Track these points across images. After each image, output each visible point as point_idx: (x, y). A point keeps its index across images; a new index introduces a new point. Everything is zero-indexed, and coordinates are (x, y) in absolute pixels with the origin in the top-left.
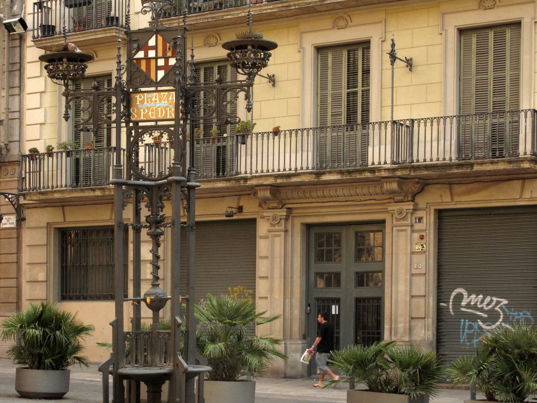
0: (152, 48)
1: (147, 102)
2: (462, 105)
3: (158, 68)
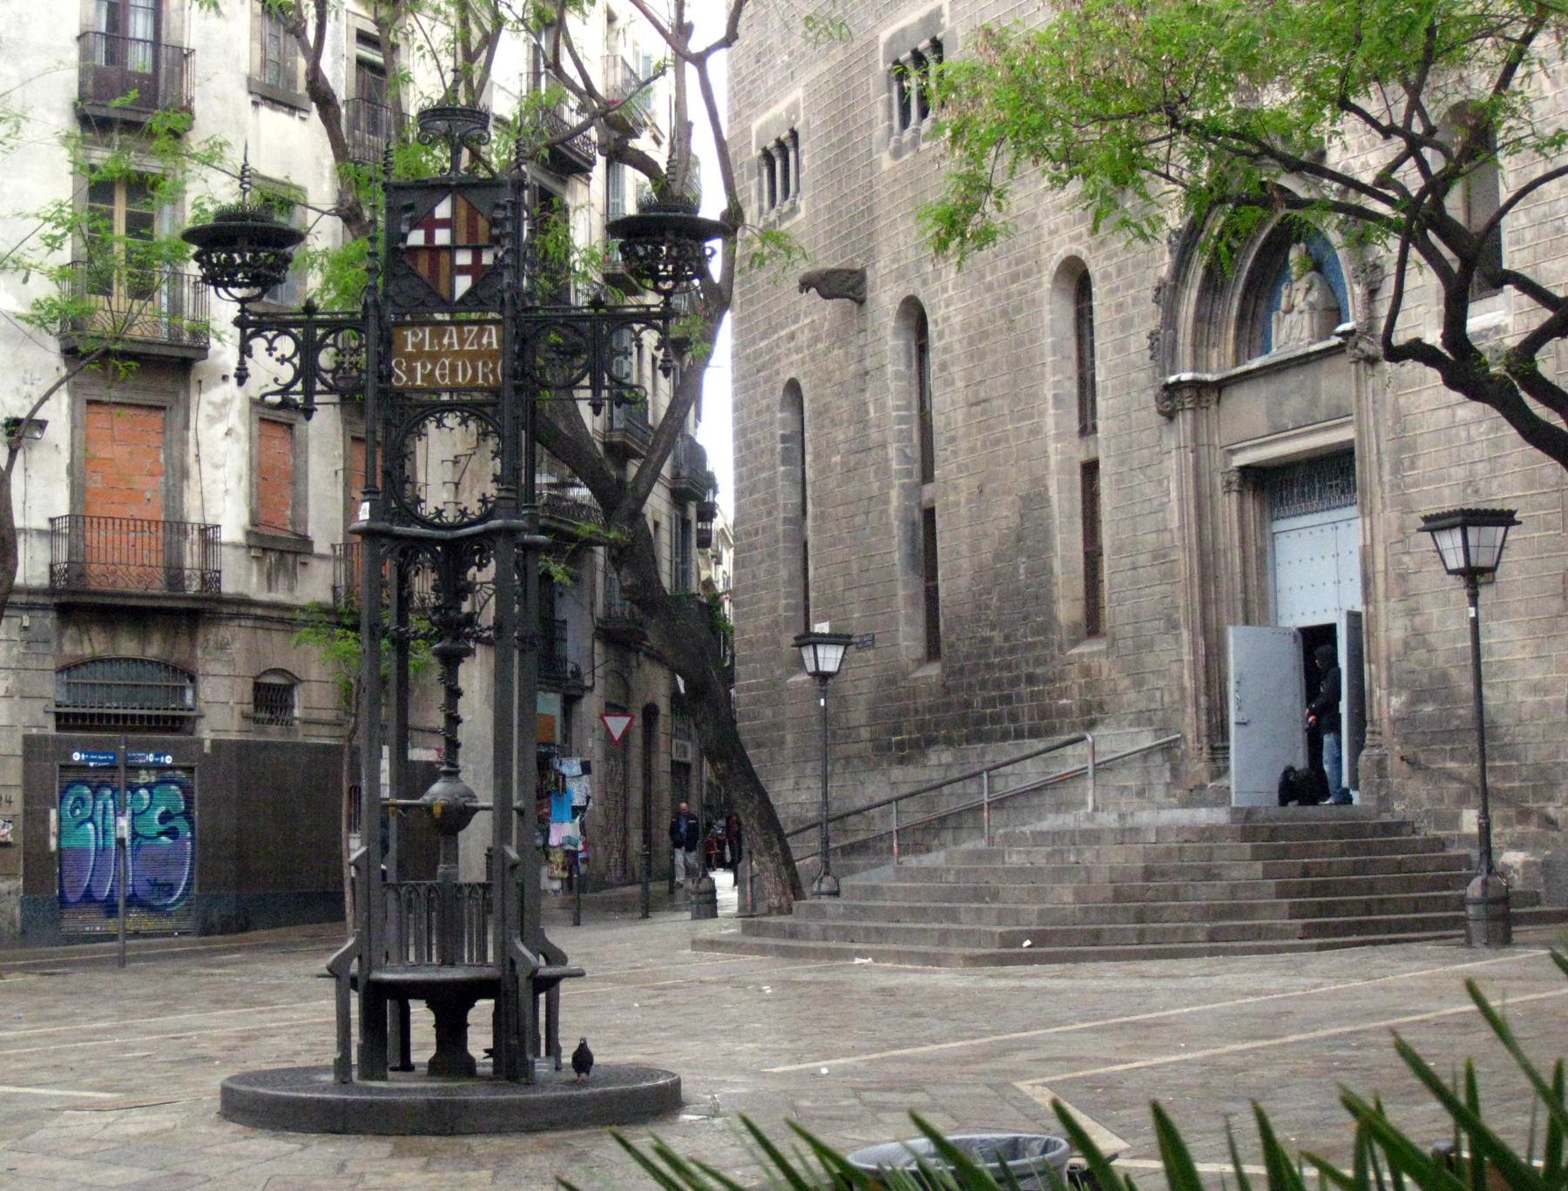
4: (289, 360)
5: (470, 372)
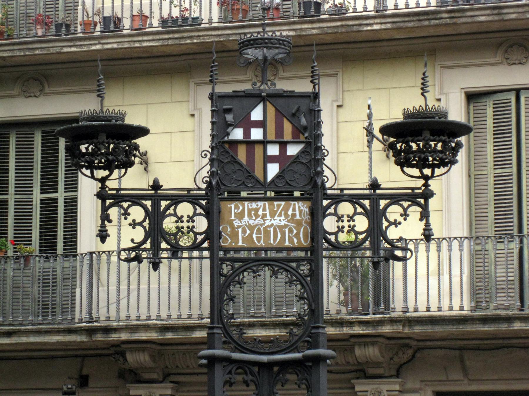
1: (250, 216)
2: (473, 218)
4: (405, 210)
5: (279, 236)
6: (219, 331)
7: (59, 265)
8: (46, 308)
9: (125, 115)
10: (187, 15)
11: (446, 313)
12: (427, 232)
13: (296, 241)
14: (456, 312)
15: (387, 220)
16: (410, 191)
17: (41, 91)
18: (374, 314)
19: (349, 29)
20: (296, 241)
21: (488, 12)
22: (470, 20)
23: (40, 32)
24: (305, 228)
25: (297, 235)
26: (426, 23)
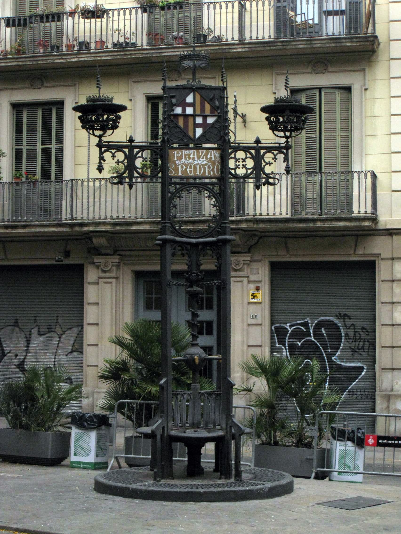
0: (190, 105)
1: (185, 158)
3: (196, 125)
4: (275, 156)
5: (202, 170)
6: (169, 225)
7: (53, 187)
8: (46, 211)
9: (113, 99)
10: (128, 41)
11: (278, 216)
12: (287, 169)
13: (212, 173)
14: (284, 216)
15: (264, 161)
16: (278, 145)
17: (42, 85)
18: (237, 217)
19: (224, 51)
20: (212, 173)
21: (304, 43)
22: (294, 47)
23: (42, 51)
24: (218, 166)
25: (213, 170)
26: (268, 48)
